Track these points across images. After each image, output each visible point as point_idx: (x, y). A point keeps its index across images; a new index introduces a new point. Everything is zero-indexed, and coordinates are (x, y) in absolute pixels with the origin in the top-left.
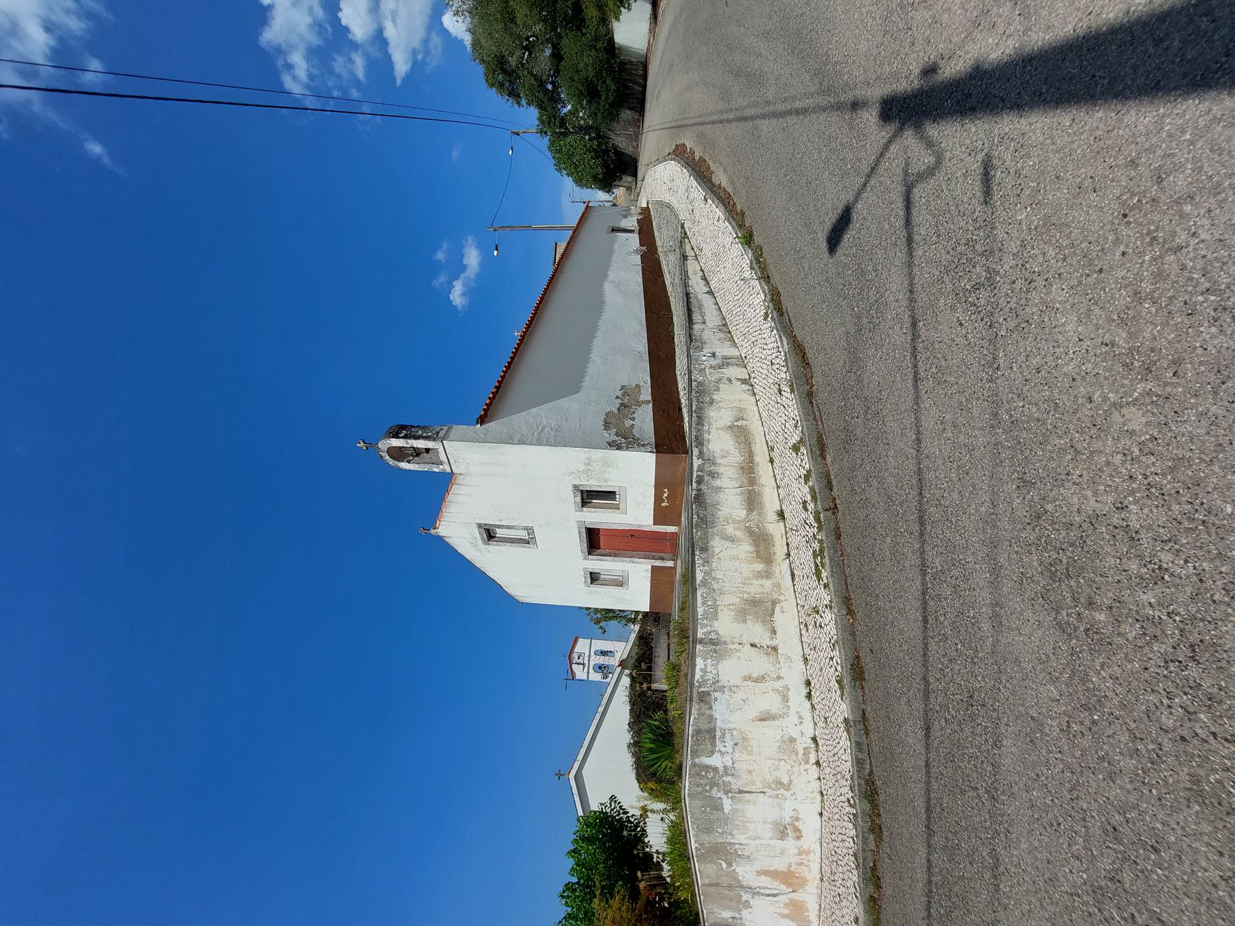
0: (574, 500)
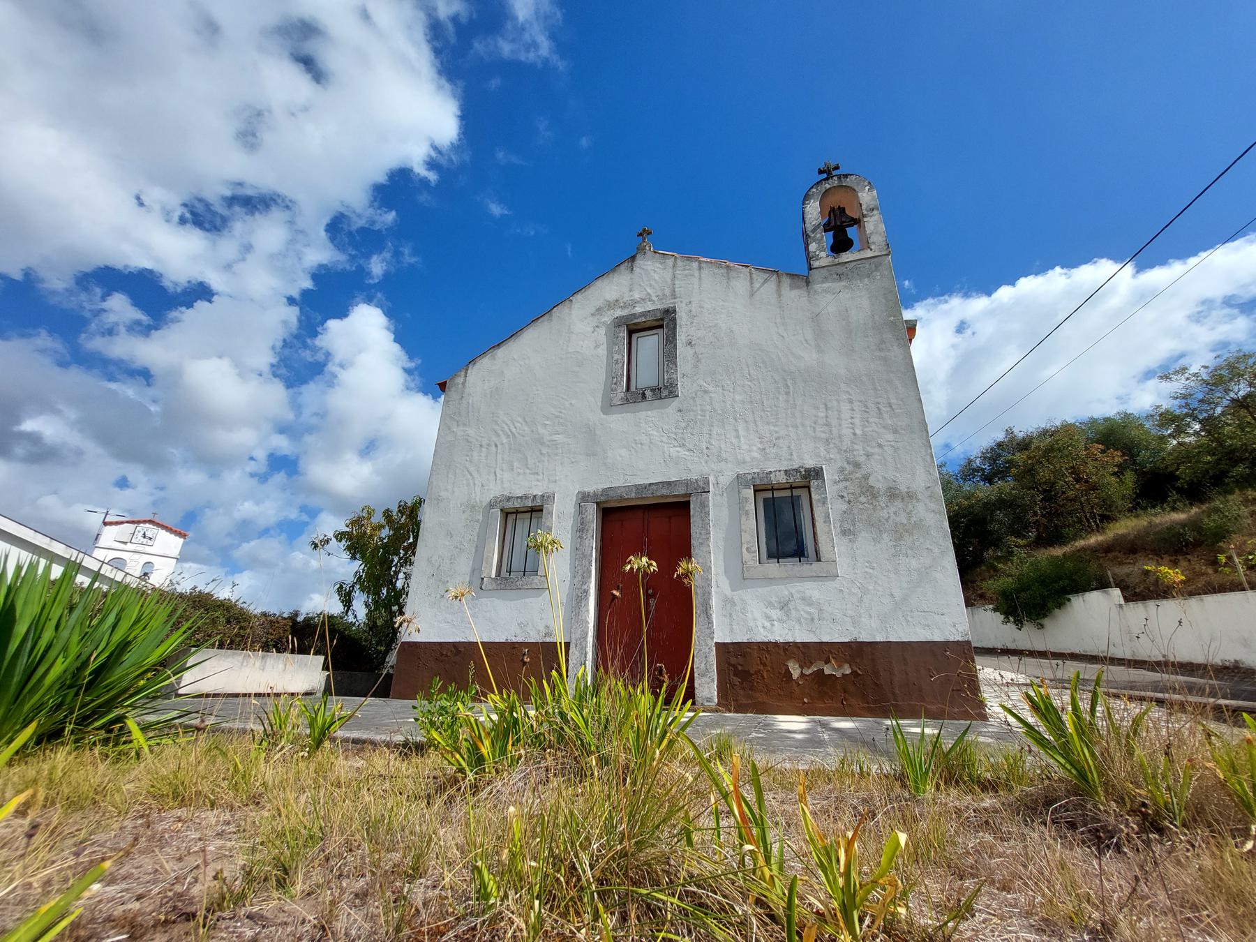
0: (777, 467)
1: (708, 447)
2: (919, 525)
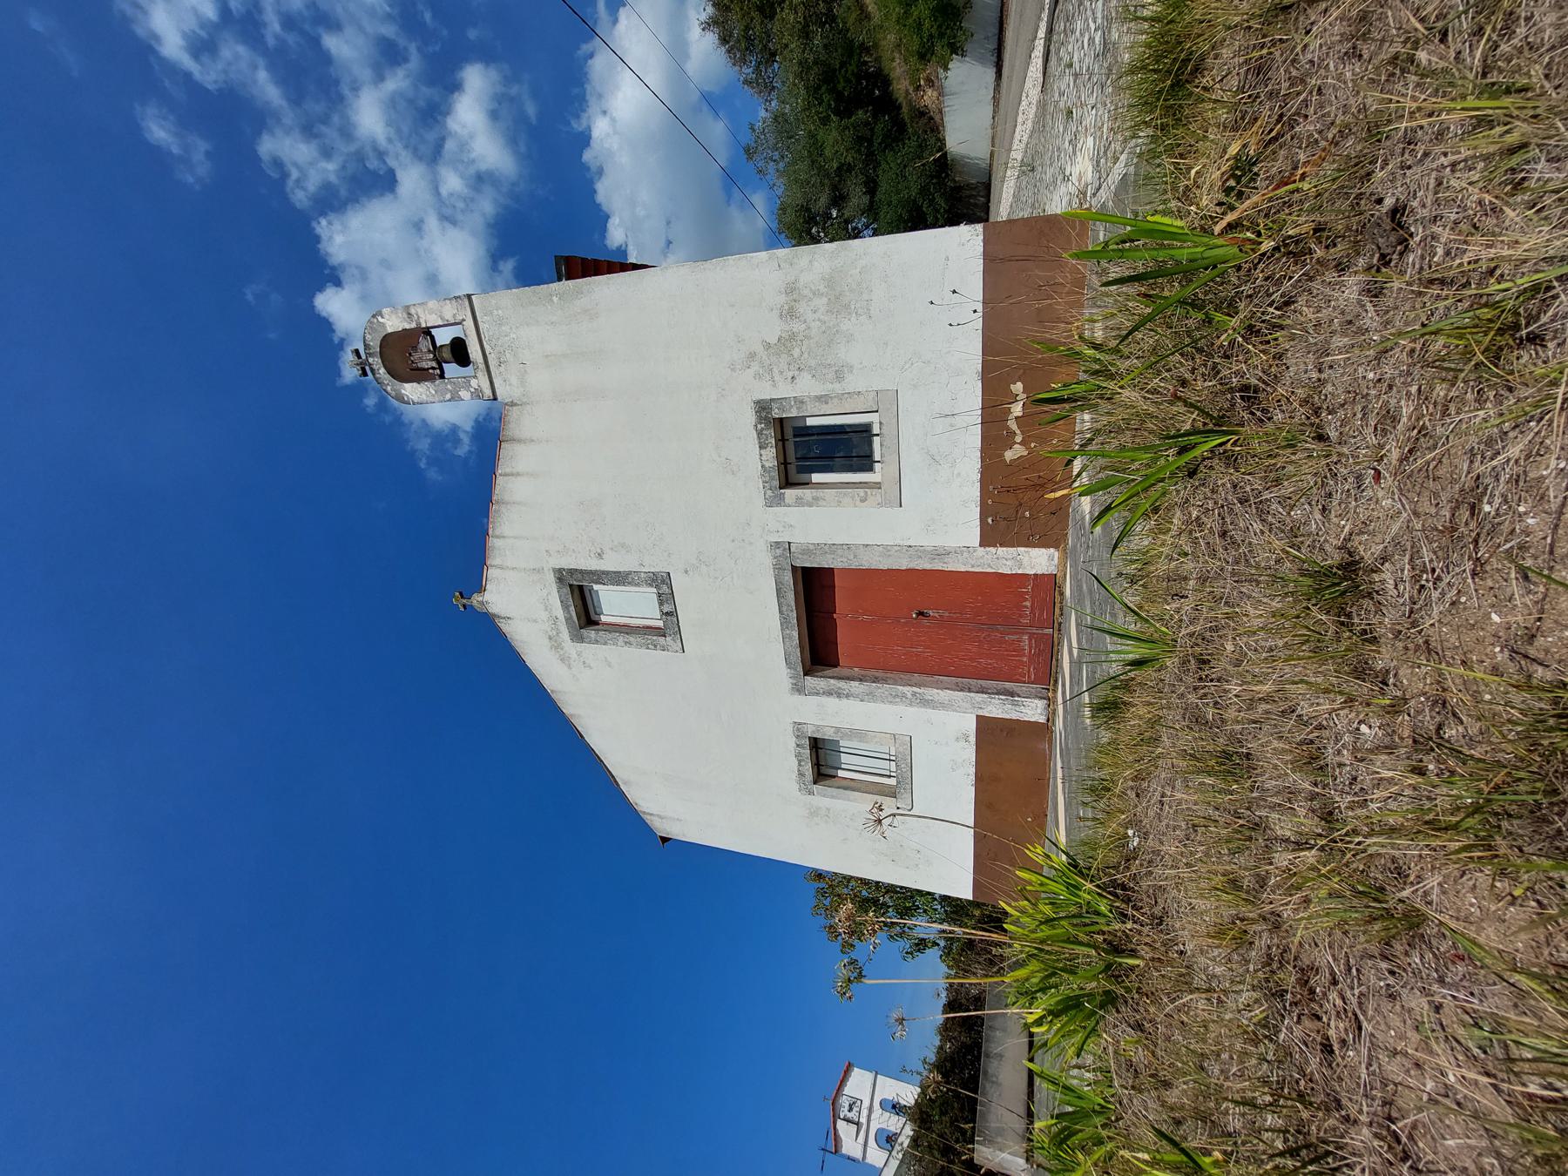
0: (754, 457)
1: (735, 543)
2: (830, 282)
